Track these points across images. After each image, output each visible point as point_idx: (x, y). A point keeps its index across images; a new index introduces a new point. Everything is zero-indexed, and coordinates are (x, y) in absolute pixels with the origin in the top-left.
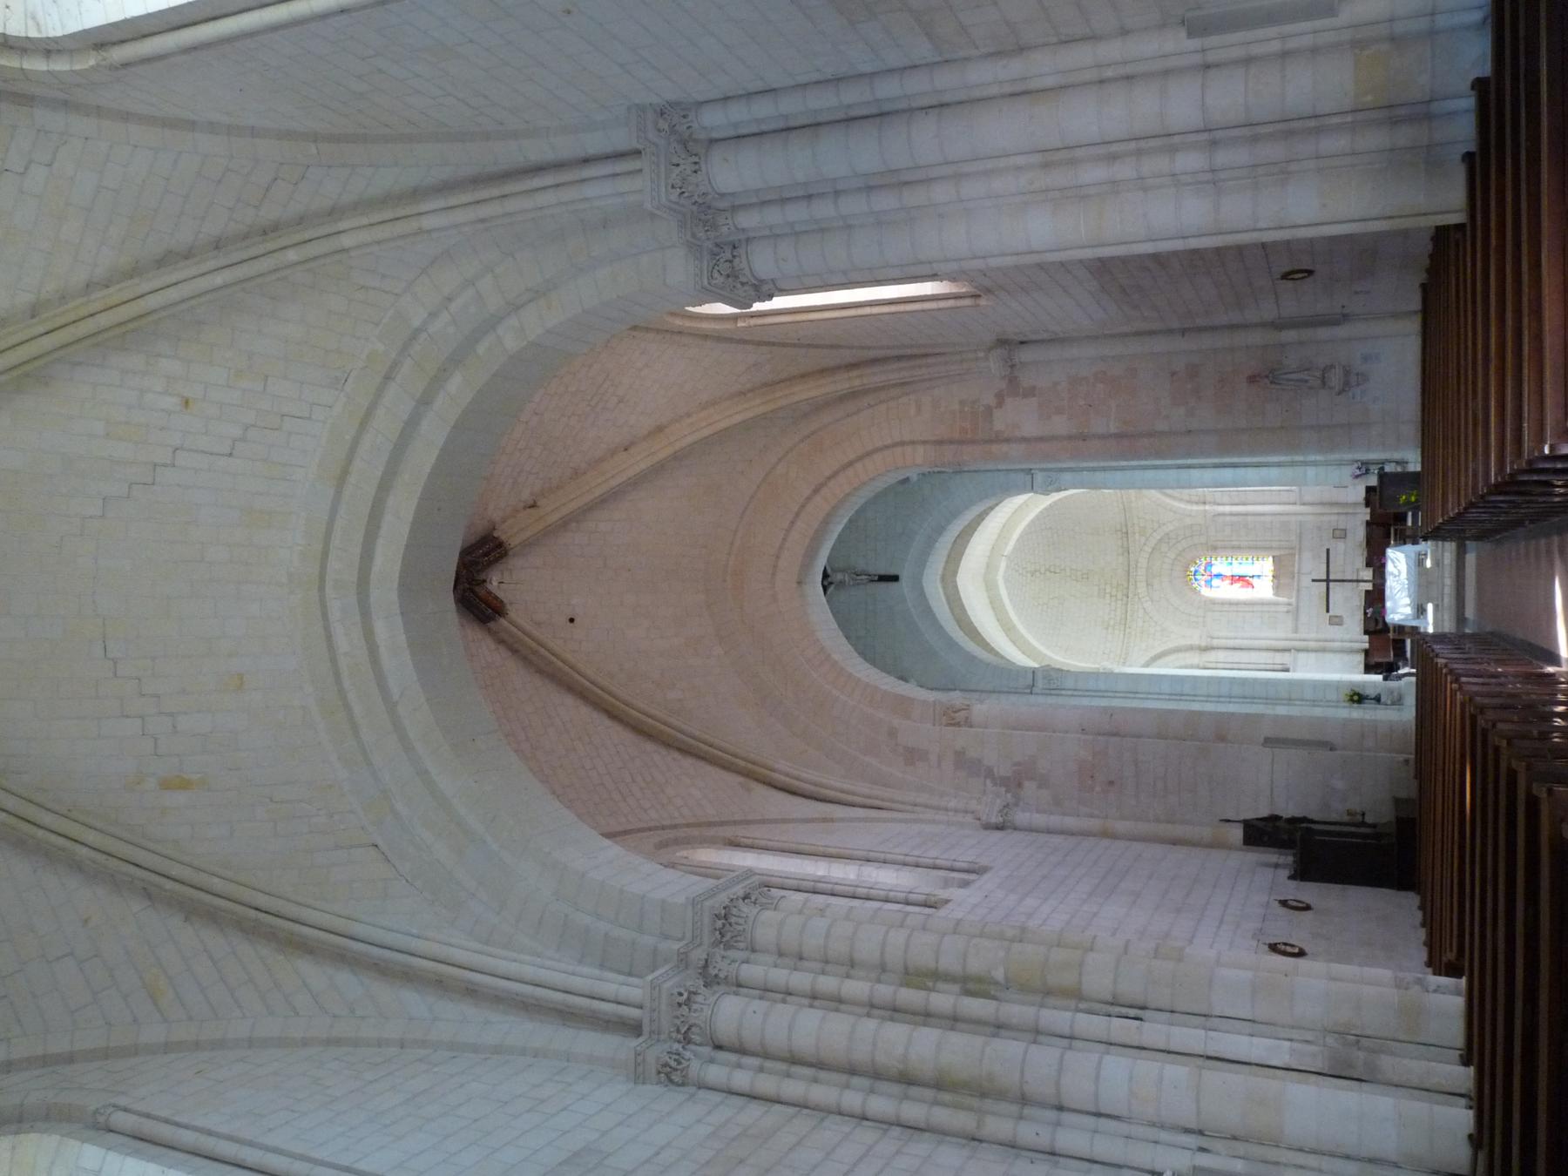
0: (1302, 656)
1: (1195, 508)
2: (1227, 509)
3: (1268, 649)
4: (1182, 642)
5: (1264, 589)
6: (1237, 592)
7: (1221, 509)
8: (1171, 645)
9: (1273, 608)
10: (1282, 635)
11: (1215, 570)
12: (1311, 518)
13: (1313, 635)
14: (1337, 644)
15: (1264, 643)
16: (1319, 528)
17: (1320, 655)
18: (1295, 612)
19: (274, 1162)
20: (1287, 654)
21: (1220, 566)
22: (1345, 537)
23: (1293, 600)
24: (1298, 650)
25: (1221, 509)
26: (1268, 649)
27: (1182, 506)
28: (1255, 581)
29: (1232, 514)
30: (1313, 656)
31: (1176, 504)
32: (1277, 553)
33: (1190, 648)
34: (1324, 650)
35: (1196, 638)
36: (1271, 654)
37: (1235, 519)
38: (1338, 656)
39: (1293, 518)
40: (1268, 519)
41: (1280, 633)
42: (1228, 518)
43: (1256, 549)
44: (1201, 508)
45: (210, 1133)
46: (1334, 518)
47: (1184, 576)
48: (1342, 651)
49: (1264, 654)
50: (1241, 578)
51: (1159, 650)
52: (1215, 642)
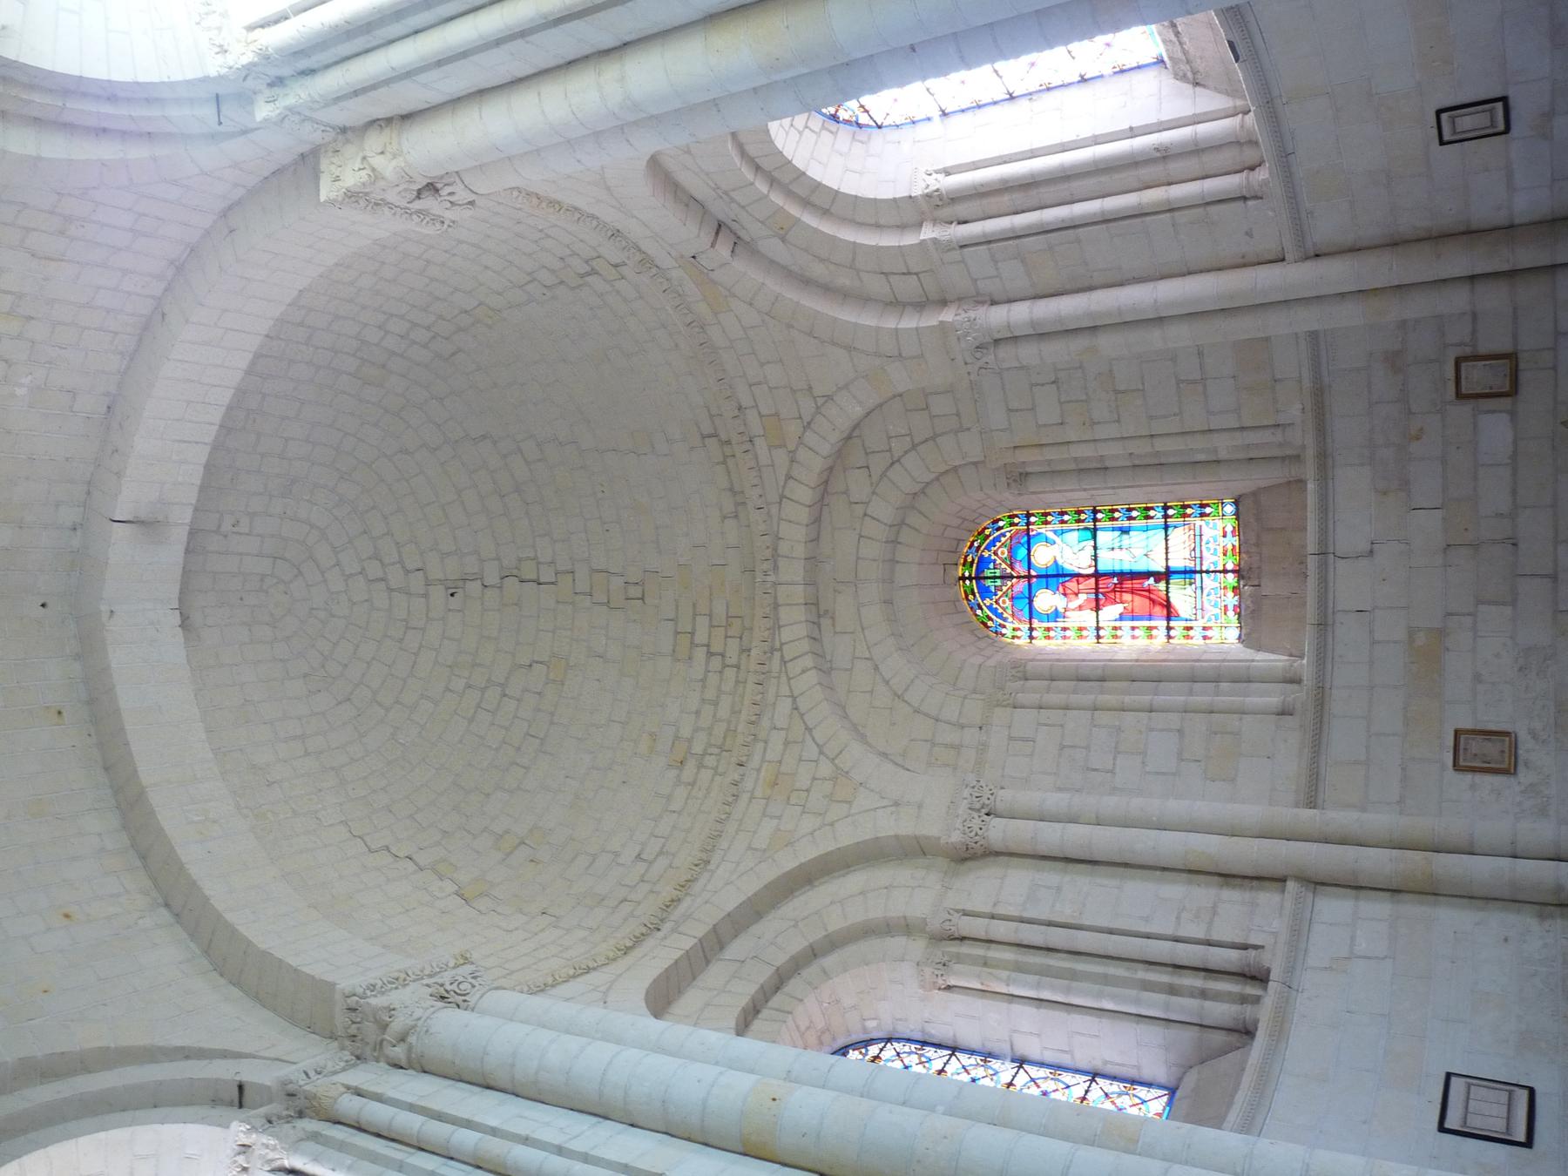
0: (1332, 908)
1: (909, 322)
2: (1020, 313)
3: (1194, 872)
4: (888, 826)
5: (1209, 621)
6: (1131, 639)
7: (997, 317)
8: (847, 836)
9: (1227, 697)
10: (1251, 812)
11: (1043, 556)
12: (1349, 315)
13: (1380, 821)
14: (1482, 869)
15: (1171, 845)
16: (1394, 361)
17: (1412, 909)
18: (1312, 711)
19: (495, 1148)
20: (1267, 898)
21: (1061, 548)
22: (1513, 391)
23: (1305, 666)
24: (1317, 883)
25: (997, 317)
26: (1194, 872)
27: (868, 319)
28: (1180, 595)
29: (1041, 334)
30: (1377, 909)
31: (848, 315)
32: (1247, 481)
33: (913, 850)
34: (1430, 891)
35: (935, 811)
36: (1203, 894)
37: (1056, 350)
38: (1498, 921)
39: (1278, 325)
40: (1180, 336)
41: (1249, 801)
42: (1028, 353)
43: (1160, 474)
44: (931, 320)
45: (440, 1117)
46: (1457, 300)
47: (973, 572)
48: (1511, 899)
49: (1174, 890)
50: (1128, 580)
51: (808, 852)
52: (998, 831)
